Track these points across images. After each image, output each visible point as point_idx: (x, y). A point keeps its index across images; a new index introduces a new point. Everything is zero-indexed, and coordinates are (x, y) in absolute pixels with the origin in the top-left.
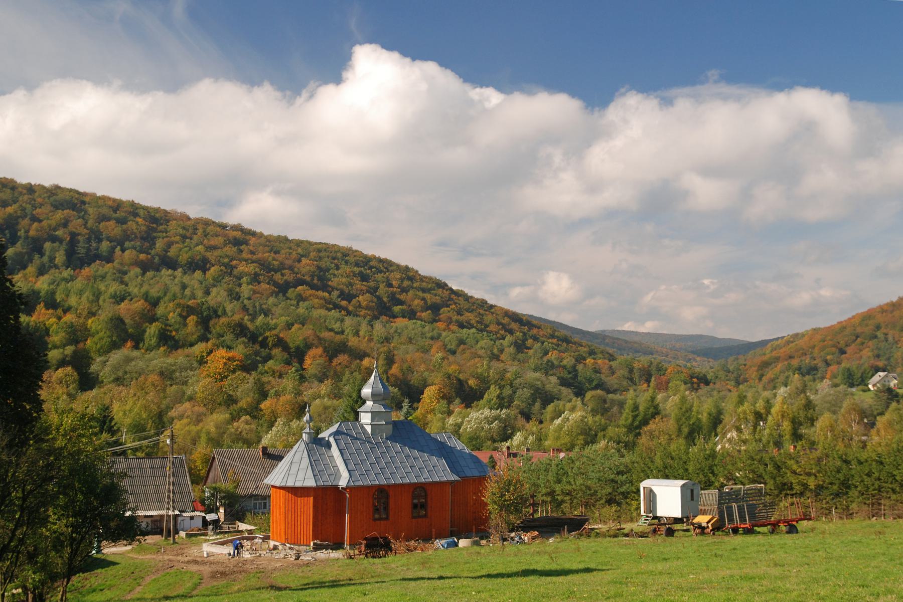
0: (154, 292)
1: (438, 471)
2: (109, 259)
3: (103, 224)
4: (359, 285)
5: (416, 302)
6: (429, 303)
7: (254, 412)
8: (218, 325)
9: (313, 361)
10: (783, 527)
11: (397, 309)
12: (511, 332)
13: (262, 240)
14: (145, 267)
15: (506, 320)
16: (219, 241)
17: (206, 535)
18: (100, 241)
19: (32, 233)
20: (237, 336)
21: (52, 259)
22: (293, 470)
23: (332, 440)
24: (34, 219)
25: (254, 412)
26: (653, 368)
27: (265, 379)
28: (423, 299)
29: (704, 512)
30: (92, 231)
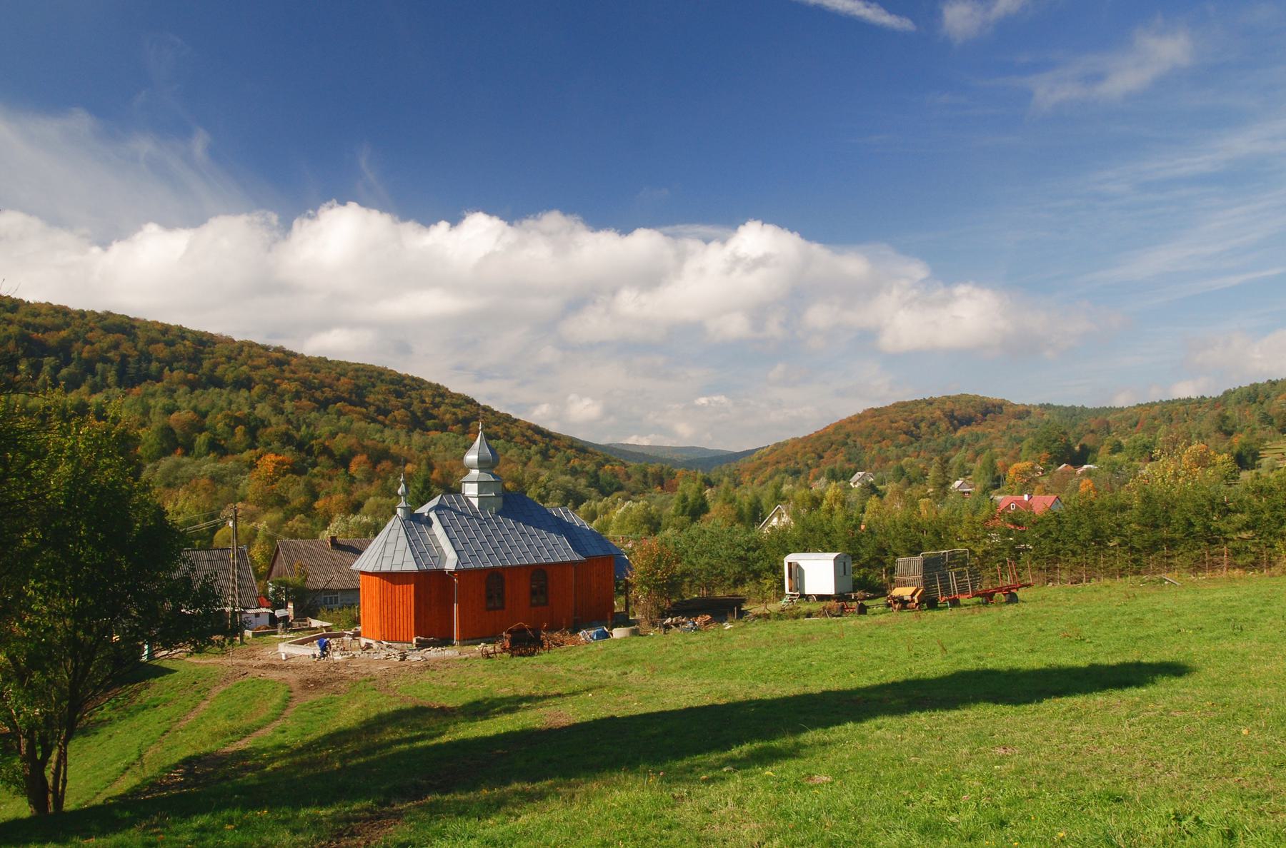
0: (203, 406)
1: (561, 551)
2: (159, 380)
3: (152, 346)
4: (394, 401)
5: (448, 416)
6: (460, 417)
7: (308, 510)
8: (264, 435)
9: (358, 466)
10: (1000, 596)
11: (430, 423)
12: (535, 442)
13: (303, 361)
14: (193, 386)
15: (530, 432)
16: (263, 361)
17: (276, 633)
18: (150, 362)
19: (85, 355)
20: (284, 444)
21: (104, 379)
22: (388, 551)
23: (433, 515)
24: (87, 342)
25: (308, 510)
26: (664, 472)
27: (316, 481)
28: (454, 414)
29: (904, 584)
30: (142, 352)
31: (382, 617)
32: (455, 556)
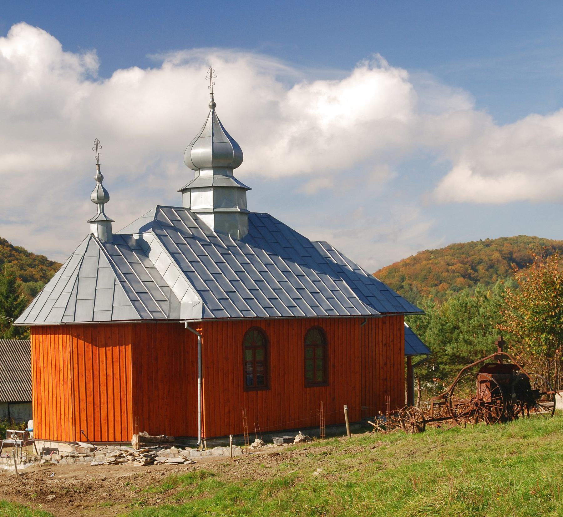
31: (77, 402)
32: (197, 298)
